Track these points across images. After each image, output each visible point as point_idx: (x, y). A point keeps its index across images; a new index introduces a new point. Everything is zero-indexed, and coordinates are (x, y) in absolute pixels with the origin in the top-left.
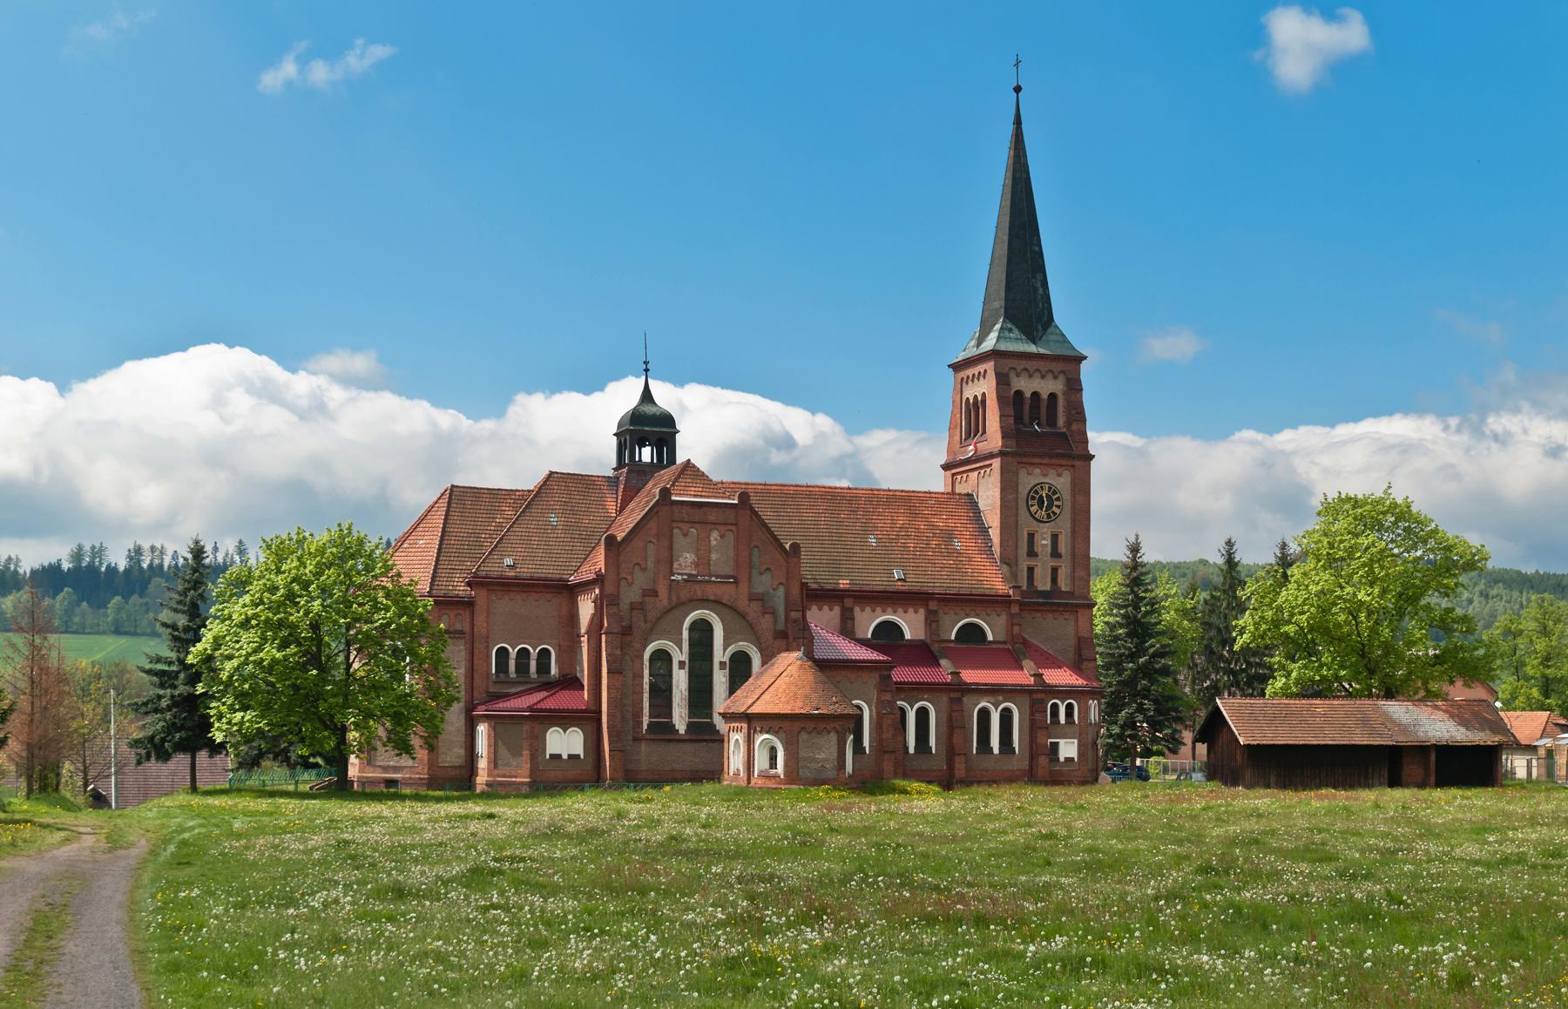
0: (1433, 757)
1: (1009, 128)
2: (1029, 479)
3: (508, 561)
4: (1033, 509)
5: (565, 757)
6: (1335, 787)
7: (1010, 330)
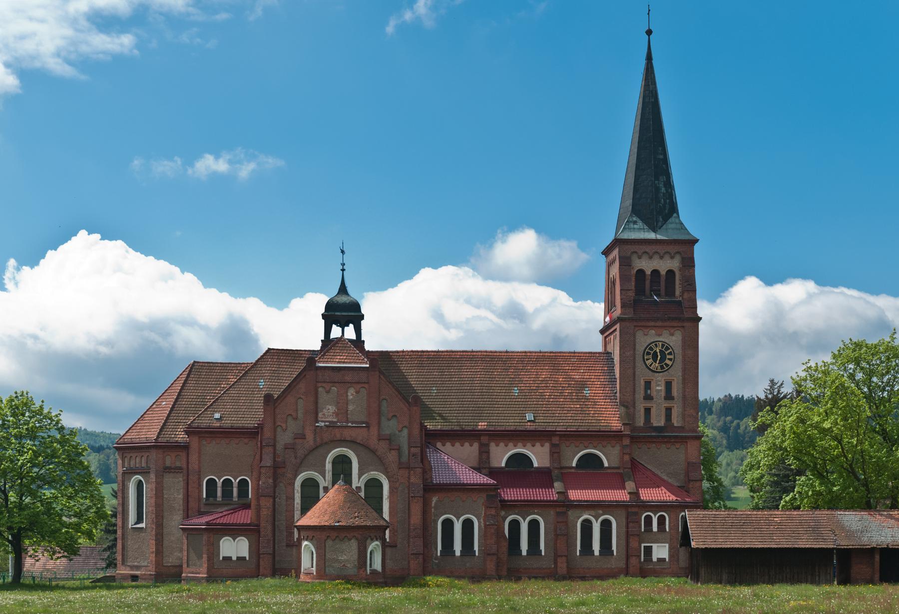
0: (877, 558)
1: (643, 62)
2: (644, 339)
3: (217, 416)
4: (649, 362)
5: (234, 558)
6: (813, 582)
7: (635, 223)
